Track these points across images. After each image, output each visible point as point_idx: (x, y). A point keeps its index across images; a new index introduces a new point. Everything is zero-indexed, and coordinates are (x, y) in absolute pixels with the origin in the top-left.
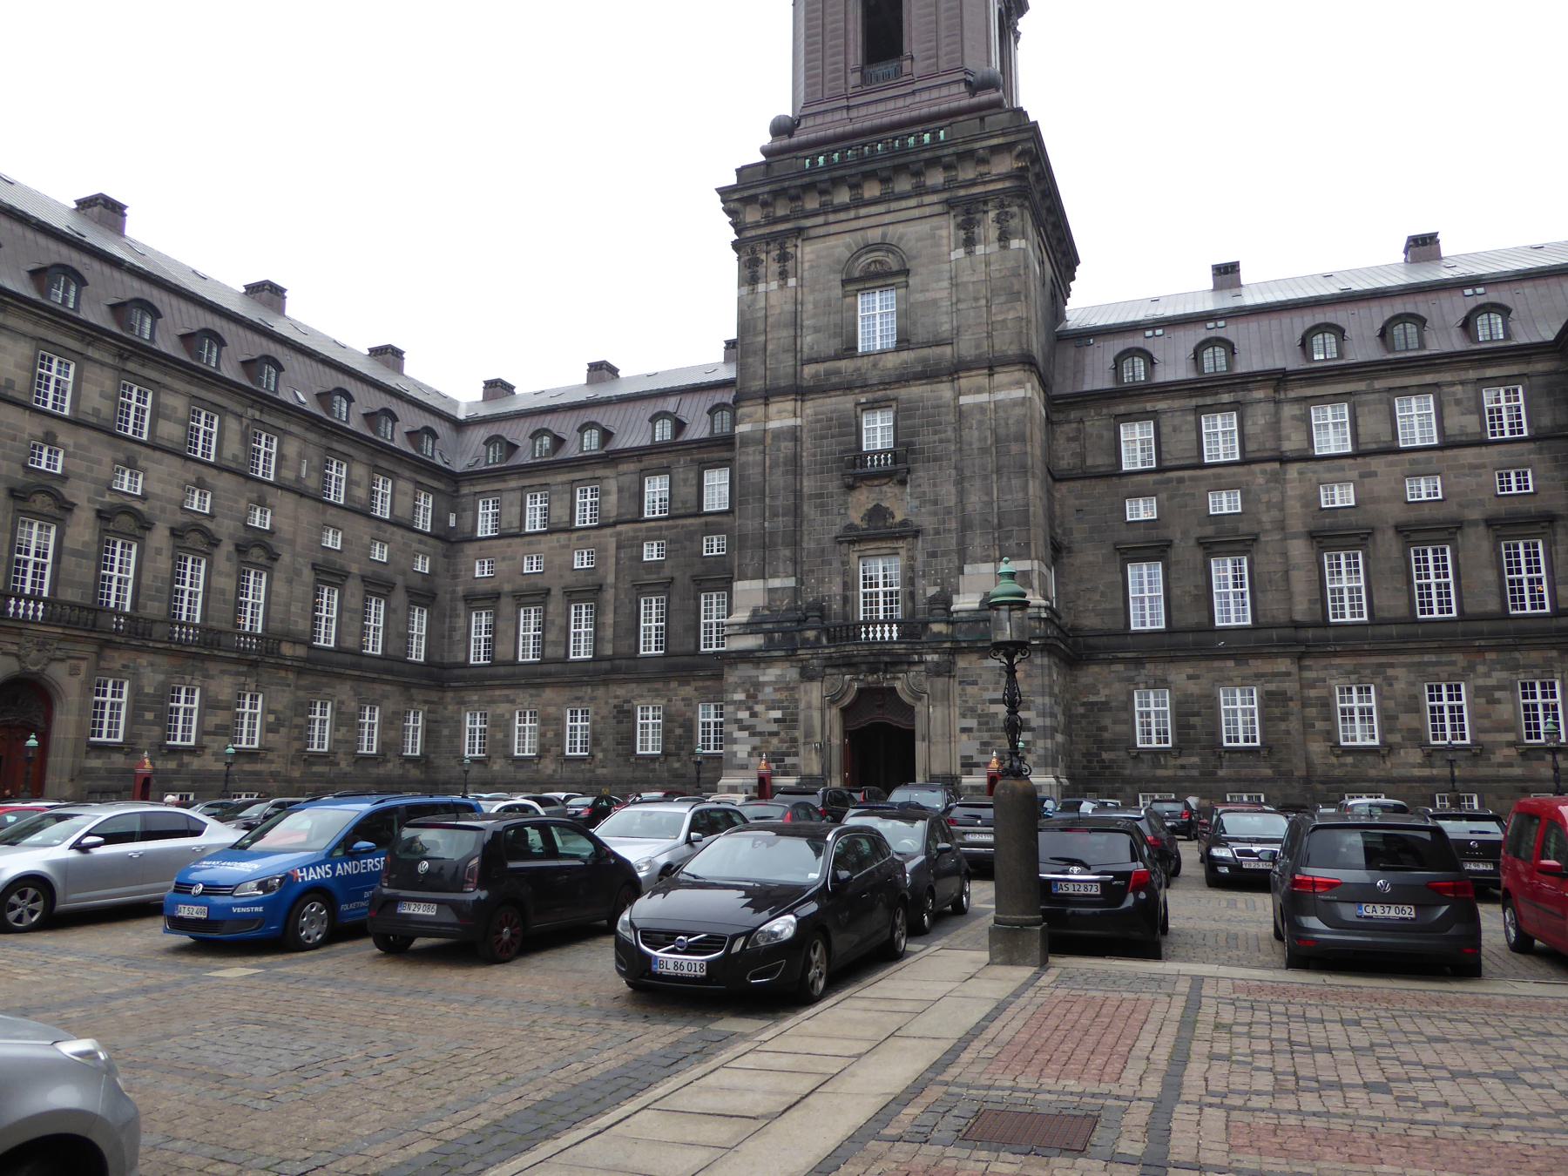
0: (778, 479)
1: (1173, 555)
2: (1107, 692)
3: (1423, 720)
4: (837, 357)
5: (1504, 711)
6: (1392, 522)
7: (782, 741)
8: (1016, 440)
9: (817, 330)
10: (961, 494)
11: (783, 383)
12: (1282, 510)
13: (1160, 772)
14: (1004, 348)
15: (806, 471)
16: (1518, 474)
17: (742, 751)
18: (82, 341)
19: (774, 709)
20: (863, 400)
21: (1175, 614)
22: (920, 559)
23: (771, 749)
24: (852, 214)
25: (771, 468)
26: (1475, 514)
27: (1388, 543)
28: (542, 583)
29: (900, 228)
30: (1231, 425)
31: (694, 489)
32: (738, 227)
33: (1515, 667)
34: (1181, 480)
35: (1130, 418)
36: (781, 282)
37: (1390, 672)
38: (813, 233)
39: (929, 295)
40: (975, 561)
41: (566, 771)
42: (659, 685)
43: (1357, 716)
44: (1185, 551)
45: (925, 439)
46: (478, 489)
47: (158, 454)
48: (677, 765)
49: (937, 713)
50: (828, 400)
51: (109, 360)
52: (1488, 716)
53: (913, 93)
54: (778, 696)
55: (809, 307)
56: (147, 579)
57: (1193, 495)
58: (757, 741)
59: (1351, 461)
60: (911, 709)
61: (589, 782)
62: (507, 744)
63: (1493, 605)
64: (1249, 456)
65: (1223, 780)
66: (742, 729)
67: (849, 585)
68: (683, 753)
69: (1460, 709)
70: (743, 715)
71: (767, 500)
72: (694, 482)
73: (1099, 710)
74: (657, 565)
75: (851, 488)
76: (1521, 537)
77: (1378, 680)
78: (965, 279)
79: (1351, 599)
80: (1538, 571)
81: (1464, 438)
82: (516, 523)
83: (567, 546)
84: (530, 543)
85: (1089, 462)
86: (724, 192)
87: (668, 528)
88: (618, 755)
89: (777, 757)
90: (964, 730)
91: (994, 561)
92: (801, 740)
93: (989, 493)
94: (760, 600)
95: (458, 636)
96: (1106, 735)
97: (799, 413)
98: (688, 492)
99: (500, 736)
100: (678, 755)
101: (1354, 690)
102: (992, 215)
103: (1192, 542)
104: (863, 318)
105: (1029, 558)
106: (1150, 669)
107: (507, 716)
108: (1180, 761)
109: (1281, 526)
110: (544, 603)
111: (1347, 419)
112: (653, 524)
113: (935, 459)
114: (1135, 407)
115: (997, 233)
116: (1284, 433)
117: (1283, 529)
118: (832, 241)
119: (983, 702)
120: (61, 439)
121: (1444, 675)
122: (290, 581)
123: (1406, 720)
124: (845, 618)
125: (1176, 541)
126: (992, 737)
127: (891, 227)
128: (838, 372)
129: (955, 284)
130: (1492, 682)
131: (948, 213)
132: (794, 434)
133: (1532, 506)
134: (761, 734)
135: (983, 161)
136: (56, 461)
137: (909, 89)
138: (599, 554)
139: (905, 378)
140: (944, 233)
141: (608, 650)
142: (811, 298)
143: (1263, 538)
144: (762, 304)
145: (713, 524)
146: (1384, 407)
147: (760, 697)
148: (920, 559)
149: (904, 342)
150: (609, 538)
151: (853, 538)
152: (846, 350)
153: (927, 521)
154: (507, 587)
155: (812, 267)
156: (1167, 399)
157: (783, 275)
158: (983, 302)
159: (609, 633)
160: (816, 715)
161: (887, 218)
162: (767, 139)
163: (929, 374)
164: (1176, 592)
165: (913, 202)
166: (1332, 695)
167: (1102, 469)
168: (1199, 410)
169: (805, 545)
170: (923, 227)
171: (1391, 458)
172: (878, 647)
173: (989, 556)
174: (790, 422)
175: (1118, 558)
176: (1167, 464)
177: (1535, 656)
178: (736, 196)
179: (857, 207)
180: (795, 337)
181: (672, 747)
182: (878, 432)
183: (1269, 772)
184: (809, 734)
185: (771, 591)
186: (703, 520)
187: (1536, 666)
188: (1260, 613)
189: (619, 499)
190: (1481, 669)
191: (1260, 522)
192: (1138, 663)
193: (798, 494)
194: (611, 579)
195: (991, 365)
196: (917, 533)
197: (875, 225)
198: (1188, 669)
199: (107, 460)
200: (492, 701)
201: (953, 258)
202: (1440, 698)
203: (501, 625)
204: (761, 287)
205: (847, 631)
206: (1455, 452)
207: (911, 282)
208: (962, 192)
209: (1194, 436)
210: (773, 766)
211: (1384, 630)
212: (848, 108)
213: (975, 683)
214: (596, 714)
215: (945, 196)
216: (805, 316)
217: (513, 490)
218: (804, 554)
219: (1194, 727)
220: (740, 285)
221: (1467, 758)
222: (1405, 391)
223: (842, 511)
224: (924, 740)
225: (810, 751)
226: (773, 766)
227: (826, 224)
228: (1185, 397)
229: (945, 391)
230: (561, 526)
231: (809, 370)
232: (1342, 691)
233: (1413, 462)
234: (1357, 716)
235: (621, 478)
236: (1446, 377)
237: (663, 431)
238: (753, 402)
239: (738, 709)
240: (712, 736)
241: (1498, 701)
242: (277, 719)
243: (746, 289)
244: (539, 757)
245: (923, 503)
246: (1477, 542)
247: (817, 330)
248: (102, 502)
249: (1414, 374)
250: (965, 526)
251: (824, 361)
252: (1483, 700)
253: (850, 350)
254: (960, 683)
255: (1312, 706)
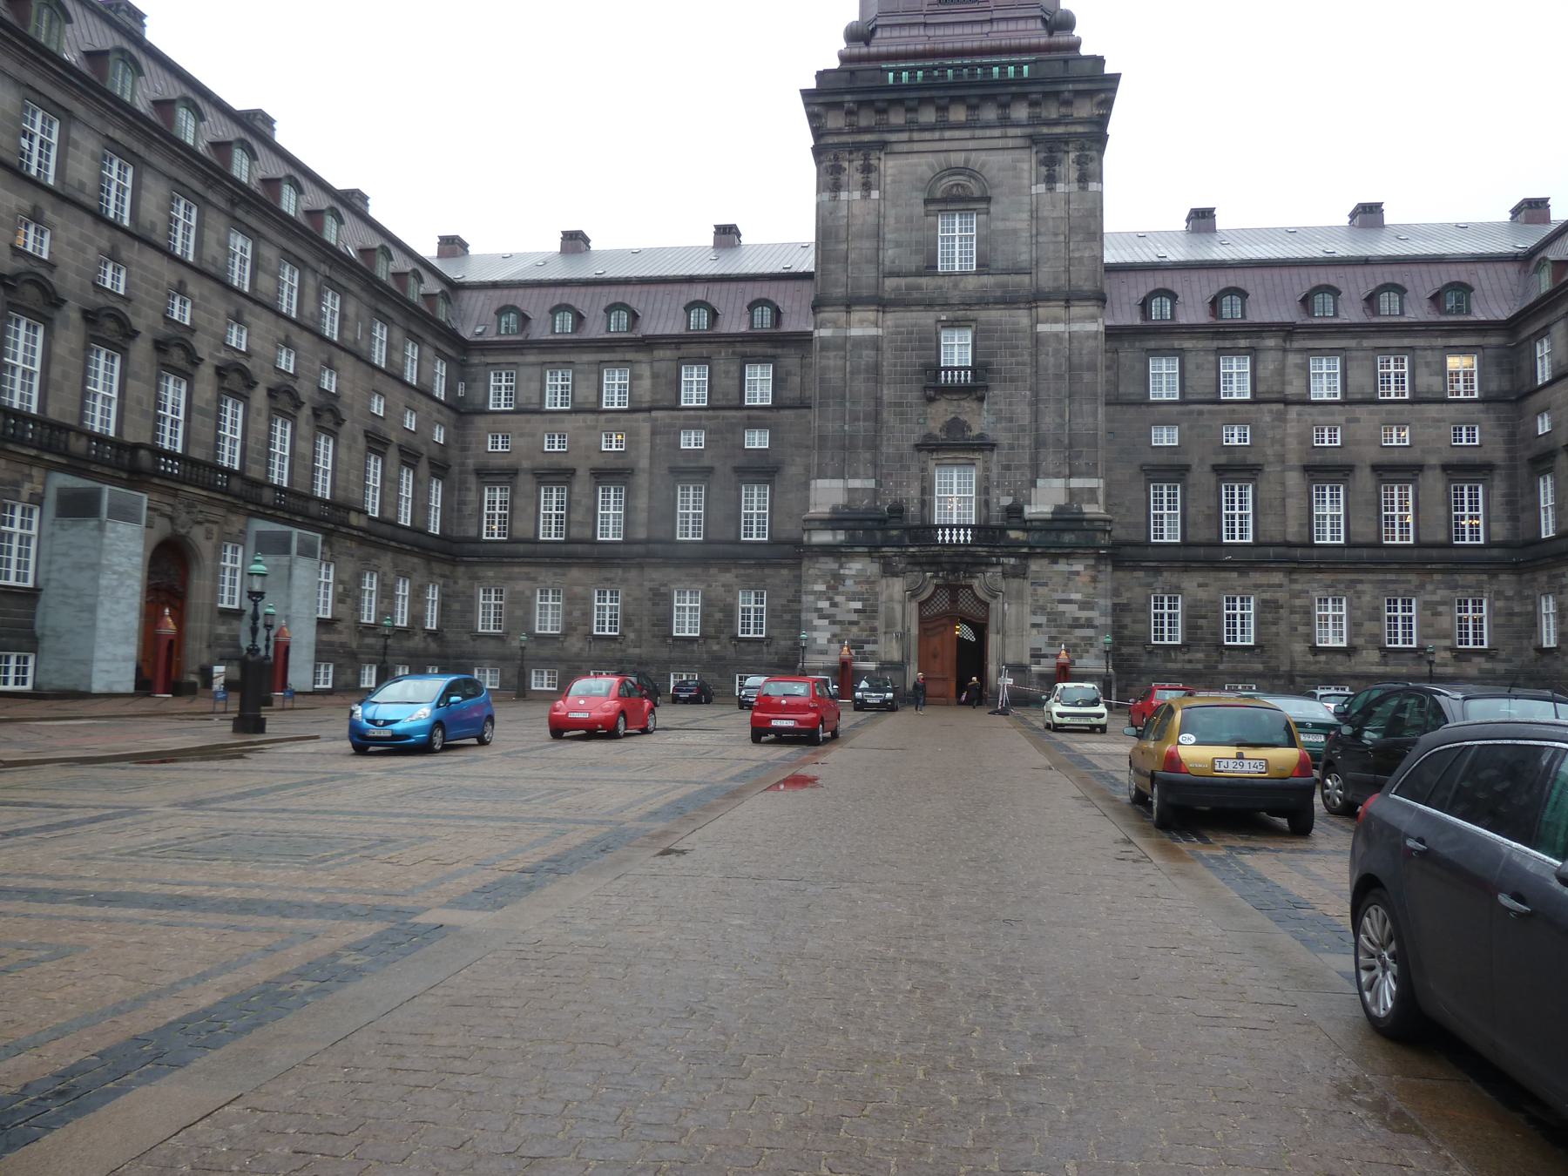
0: (860, 385)
1: (1192, 478)
2: (1128, 595)
3: (1382, 628)
4: (918, 274)
5: (1444, 622)
6: (1368, 463)
7: (863, 630)
8: (1089, 369)
9: (898, 244)
10: (1036, 416)
11: (865, 293)
12: (1283, 445)
13: (1171, 665)
14: (1081, 283)
15: (886, 379)
16: (1468, 429)
17: (822, 638)
18: (204, 183)
19: (854, 600)
20: (944, 318)
21: (1190, 531)
22: (995, 471)
23: (851, 637)
24: (937, 135)
25: (852, 373)
26: (1433, 460)
27: (1365, 479)
28: (566, 462)
29: (983, 156)
30: (966, 340)
31: (737, 382)
32: (818, 133)
33: (1454, 587)
34: (1201, 413)
35: (1159, 352)
36: (864, 193)
37: (1359, 587)
38: (897, 148)
39: (1009, 225)
40: (1047, 475)
41: (596, 650)
42: (699, 571)
43: (1330, 622)
44: (1201, 476)
45: (1002, 361)
46: (490, 359)
47: (258, 309)
48: (716, 648)
49: (1011, 610)
50: (909, 314)
51: (223, 204)
52: (1431, 625)
53: (991, 21)
54: (858, 588)
55: (891, 221)
56: (251, 443)
57: (1210, 427)
58: (837, 629)
59: (1340, 408)
60: (987, 605)
61: (620, 661)
62: (527, 622)
63: (1441, 537)
64: (1260, 396)
65: (1222, 673)
66: (822, 617)
67: (927, 490)
68: (722, 636)
69: (1410, 619)
70: (824, 604)
71: (847, 404)
72: (737, 375)
73: (1122, 610)
74: (697, 454)
75: (931, 400)
76: (1466, 481)
77: (1348, 594)
78: (1046, 214)
79: (1332, 525)
80: (1477, 509)
81: (1430, 396)
82: (535, 399)
83: (595, 428)
84: (551, 421)
85: (1122, 390)
86: (806, 94)
87: (708, 418)
88: (654, 636)
89: (857, 645)
90: (1034, 625)
91: (1064, 477)
92: (882, 629)
93: (1062, 416)
94: (840, 499)
95: (468, 510)
96: (1126, 632)
97: (880, 323)
98: (730, 384)
99: (519, 613)
100: (718, 638)
101: (1330, 601)
102: (1072, 156)
103: (1207, 468)
104: (942, 238)
105: (1096, 477)
106: (1168, 577)
107: (528, 593)
108: (1187, 657)
109: (1281, 459)
110: (568, 483)
111: (1338, 371)
112: (692, 413)
113: (1012, 380)
114: (1165, 344)
115: (1076, 175)
116: (1287, 378)
117: (1283, 462)
118: (914, 159)
119: (1053, 601)
120: (191, 288)
121: (1401, 592)
122: (349, 448)
123: (1369, 627)
124: (923, 518)
125: (1194, 467)
126: (1060, 632)
127: (974, 154)
128: (918, 288)
129: (1035, 216)
130: (1436, 598)
131: (1030, 147)
132: (875, 343)
133: (1477, 457)
134: (841, 623)
135: (1068, 103)
136: (1474, 435)
137: (987, 16)
138: (632, 435)
139: (983, 301)
140: (1026, 166)
141: (641, 534)
142: (893, 212)
143: (1267, 469)
144: (845, 213)
145: (758, 418)
146: (594, 377)
147: (841, 588)
148: (995, 471)
149: (984, 267)
150: (643, 424)
151: (929, 446)
152: (927, 267)
153: (1003, 438)
154: (526, 464)
155: (894, 182)
156: (1192, 338)
157: (867, 187)
158: (1062, 238)
159: (642, 517)
160: (898, 608)
161: (971, 144)
162: (842, 45)
163: (1009, 300)
164: (1191, 511)
165: (997, 132)
166: (1313, 604)
167: (1132, 397)
168: (1220, 351)
169: (884, 449)
170: (1007, 157)
171: (1372, 407)
172: (962, 549)
173: (1059, 472)
174: (872, 331)
175: (1143, 478)
176: (1190, 397)
177: (1471, 579)
178: (821, 100)
179: (942, 129)
180: (878, 249)
181: (712, 631)
182: (957, 350)
183: (1259, 667)
184: (890, 624)
185: (851, 491)
186: (745, 413)
187: (1470, 587)
188: (1260, 533)
189: (654, 386)
190: (1429, 587)
191: (1265, 455)
192: (1157, 571)
193: (878, 401)
194: (644, 463)
195: (1069, 298)
196: (992, 446)
197: (959, 148)
198: (1198, 578)
199: (222, 313)
200: (510, 578)
201: (1034, 191)
202: (1162, 607)
203: (519, 502)
204: (844, 195)
205: (925, 531)
206: (1423, 406)
207: (992, 210)
208: (1045, 130)
209: (1214, 374)
210: (853, 652)
211: (1357, 552)
212: (925, 25)
213: (1045, 584)
214: (628, 595)
215: (1029, 131)
216: (886, 229)
217: (533, 364)
218: (883, 458)
219: (1201, 628)
220: (818, 192)
221: (1414, 659)
222: (1385, 350)
223: (921, 421)
224: (998, 633)
225: (891, 640)
226: (853, 652)
227: (911, 141)
228: (1208, 339)
229: (1022, 318)
230: (588, 406)
231: (890, 283)
232: (1320, 600)
233: (1389, 412)
234: (1330, 622)
235: (656, 365)
236: (1420, 342)
237: (700, 320)
238: (835, 308)
239: (818, 599)
240: (752, 622)
241: (1440, 614)
242: (345, 589)
243: (826, 196)
244: (565, 635)
245: (999, 420)
246: (1434, 482)
247: (898, 244)
248: (219, 358)
249: (1395, 337)
250: (1039, 443)
251: (906, 276)
252: (1429, 613)
253: (930, 268)
254: (1032, 584)
255: (1296, 613)
